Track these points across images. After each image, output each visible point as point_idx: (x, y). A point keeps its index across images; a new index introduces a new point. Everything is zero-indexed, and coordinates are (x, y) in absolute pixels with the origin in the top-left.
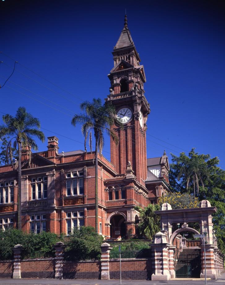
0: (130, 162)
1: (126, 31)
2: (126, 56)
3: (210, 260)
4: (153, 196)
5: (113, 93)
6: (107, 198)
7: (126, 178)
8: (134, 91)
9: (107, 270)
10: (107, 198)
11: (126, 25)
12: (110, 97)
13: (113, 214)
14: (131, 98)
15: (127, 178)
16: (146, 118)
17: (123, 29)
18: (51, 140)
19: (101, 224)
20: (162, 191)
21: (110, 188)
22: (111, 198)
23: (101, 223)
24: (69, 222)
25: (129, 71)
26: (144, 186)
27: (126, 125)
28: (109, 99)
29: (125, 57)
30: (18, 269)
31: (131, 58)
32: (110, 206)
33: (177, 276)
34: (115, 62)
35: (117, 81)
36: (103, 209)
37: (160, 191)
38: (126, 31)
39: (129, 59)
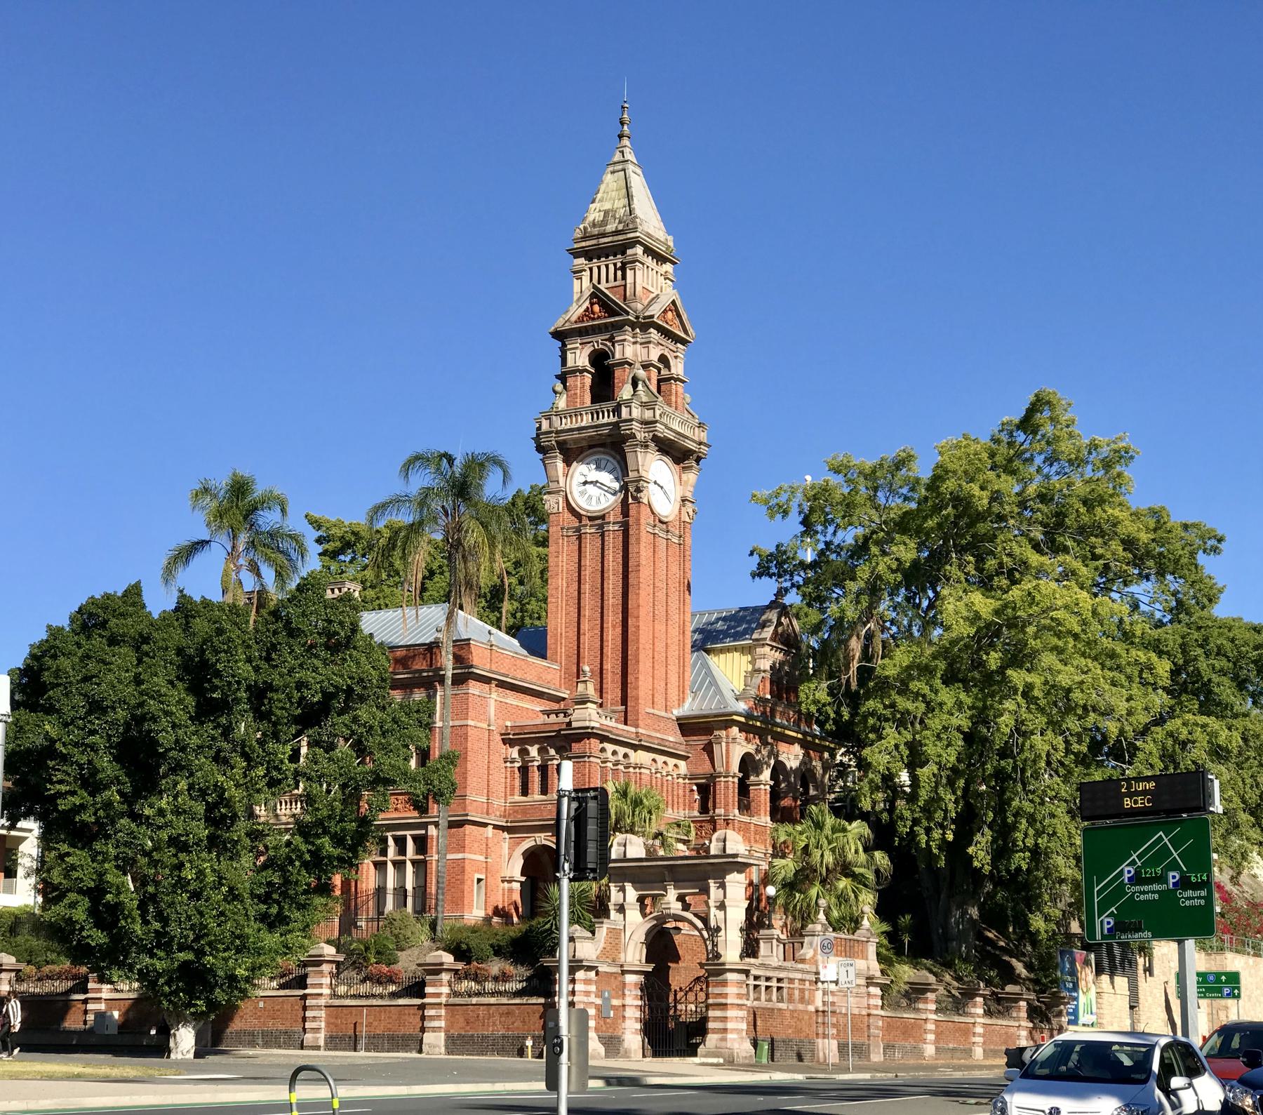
0: (587, 668)
1: (620, 167)
2: (615, 265)
3: (724, 1019)
4: (706, 768)
5: (562, 403)
6: (513, 789)
7: (569, 724)
8: (628, 404)
9: (317, 1030)
10: (513, 789)
11: (626, 142)
12: (549, 418)
13: (528, 844)
14: (616, 425)
15: (574, 725)
16: (691, 477)
17: (613, 155)
18: (336, 591)
19: (479, 880)
20: (189, 956)
21: (524, 753)
22: (525, 791)
23: (483, 877)
24: (399, 865)
25: (618, 327)
26: (673, 737)
27: (603, 517)
28: (545, 426)
29: (611, 268)
30: (317, 1030)
31: (629, 273)
32: (519, 817)
33: (449, 1051)
34: (576, 283)
35: (580, 357)
36: (490, 827)
37: (727, 750)
38: (620, 167)
39: (624, 277)
